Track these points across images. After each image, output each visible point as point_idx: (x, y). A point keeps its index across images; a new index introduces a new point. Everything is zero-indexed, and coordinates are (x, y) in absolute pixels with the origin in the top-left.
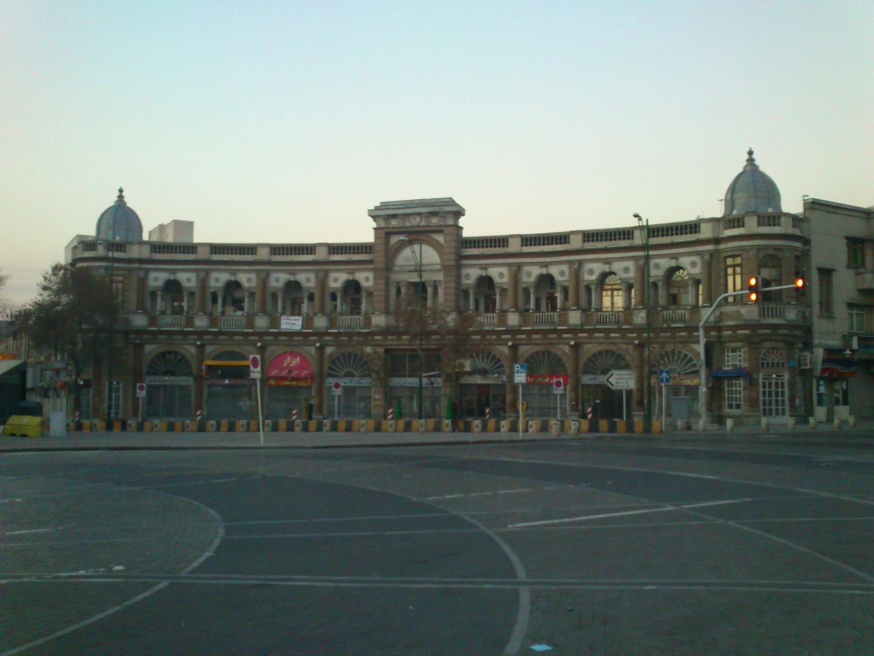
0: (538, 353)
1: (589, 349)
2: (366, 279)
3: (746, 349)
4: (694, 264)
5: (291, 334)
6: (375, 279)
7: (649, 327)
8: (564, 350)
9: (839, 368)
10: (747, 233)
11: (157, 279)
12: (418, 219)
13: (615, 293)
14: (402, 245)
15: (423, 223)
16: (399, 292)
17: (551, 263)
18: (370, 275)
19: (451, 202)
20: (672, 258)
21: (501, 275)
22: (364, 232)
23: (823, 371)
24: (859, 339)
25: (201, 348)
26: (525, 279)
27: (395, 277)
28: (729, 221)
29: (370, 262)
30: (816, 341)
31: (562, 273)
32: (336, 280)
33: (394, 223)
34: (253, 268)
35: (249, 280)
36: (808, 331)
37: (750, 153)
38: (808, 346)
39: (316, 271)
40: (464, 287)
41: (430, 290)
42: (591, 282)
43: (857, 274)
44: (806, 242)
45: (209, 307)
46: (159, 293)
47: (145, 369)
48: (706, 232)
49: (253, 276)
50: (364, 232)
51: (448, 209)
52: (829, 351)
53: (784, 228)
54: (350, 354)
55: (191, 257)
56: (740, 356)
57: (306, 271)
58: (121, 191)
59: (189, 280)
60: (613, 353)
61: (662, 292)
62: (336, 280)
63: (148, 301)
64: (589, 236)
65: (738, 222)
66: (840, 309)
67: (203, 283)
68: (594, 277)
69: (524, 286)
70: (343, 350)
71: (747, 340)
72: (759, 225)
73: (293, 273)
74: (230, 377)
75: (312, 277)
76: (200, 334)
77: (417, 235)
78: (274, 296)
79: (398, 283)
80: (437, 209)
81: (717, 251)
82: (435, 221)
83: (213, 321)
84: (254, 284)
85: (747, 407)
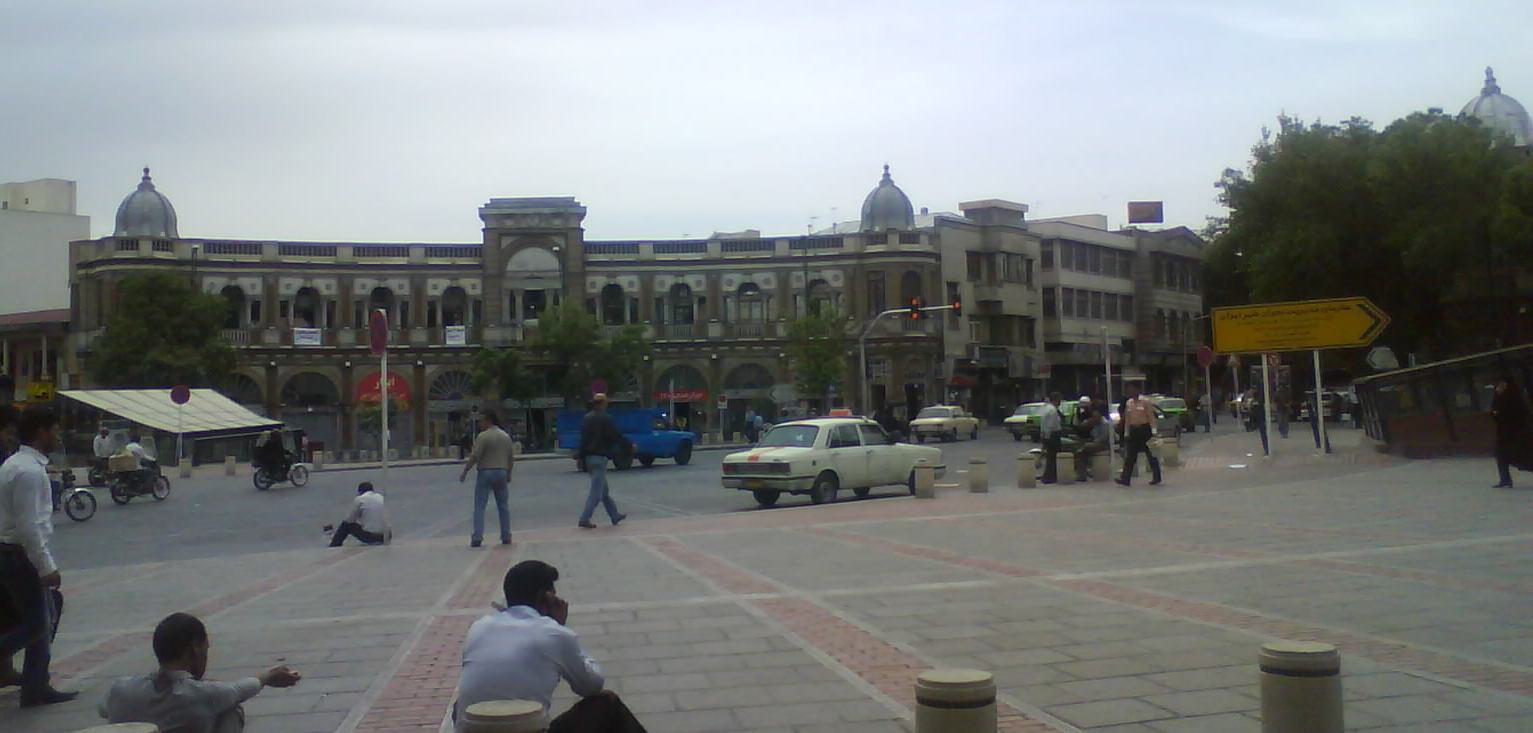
1: (731, 363)
2: (471, 286)
3: (890, 361)
4: (836, 278)
5: (309, 351)
6: (484, 288)
10: (890, 250)
13: (753, 304)
14: (515, 249)
15: (543, 225)
16: (513, 301)
18: (477, 282)
19: (569, 203)
20: (746, 274)
22: (472, 233)
23: (954, 379)
25: (271, 370)
26: (283, 291)
27: (508, 285)
28: (869, 237)
31: (699, 283)
35: (328, 287)
38: (941, 357)
43: (975, 286)
44: (938, 257)
47: (427, 392)
48: (849, 247)
49: (333, 282)
50: (472, 233)
51: (573, 210)
54: (455, 373)
55: (255, 259)
56: (884, 367)
57: (400, 275)
58: (147, 171)
59: (253, 286)
60: (756, 365)
61: (801, 301)
62: (435, 287)
65: (882, 238)
67: (270, 289)
68: (733, 288)
70: (449, 368)
72: (900, 242)
74: (312, 404)
75: (406, 283)
78: (284, 306)
79: (512, 292)
82: (557, 222)
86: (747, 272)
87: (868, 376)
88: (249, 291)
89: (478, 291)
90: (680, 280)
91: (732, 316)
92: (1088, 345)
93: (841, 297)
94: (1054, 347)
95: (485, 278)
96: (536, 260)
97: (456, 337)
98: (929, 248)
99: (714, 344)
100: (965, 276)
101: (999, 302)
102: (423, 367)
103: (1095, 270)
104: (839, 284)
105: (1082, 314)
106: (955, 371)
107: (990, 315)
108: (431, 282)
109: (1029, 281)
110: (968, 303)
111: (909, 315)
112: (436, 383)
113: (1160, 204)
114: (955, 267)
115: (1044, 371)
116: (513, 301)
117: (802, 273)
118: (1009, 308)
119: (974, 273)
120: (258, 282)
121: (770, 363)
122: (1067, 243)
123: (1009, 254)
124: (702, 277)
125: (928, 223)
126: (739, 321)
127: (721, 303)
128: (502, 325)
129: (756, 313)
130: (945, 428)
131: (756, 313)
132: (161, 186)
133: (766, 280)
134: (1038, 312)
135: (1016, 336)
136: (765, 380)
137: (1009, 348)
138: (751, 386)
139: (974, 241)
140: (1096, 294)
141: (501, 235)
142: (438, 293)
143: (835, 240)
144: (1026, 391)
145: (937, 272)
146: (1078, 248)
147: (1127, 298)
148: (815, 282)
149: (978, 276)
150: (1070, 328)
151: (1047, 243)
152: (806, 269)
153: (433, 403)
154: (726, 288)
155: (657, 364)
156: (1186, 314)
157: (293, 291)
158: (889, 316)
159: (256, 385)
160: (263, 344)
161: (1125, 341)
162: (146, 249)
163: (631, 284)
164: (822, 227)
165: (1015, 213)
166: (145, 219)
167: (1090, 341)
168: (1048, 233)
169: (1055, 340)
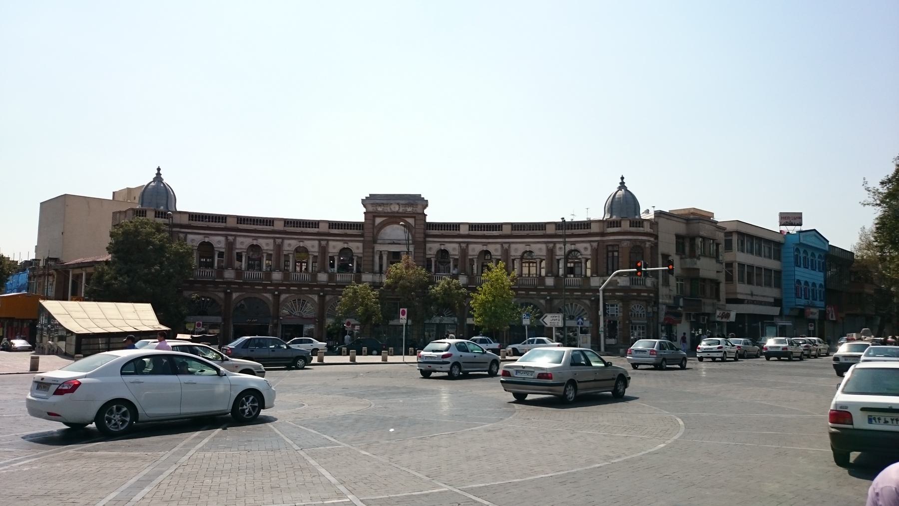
2: (356, 247)
6: (364, 248)
7: (555, 288)
9: (673, 318)
14: (383, 225)
15: (401, 210)
16: (381, 258)
17: (489, 243)
18: (360, 245)
22: (357, 215)
23: (665, 319)
24: (684, 300)
26: (470, 253)
27: (378, 248)
30: (660, 301)
33: (380, 209)
35: (267, 244)
37: (622, 178)
38: (656, 303)
40: (428, 256)
43: (681, 258)
44: (656, 237)
48: (595, 229)
50: (357, 215)
52: (668, 306)
53: (647, 228)
55: (222, 225)
63: (468, 265)
64: (515, 226)
69: (285, 253)
71: (621, 299)
73: (346, 242)
76: (229, 283)
77: (393, 218)
81: (603, 241)
86: (442, 243)
87: (605, 314)
89: (361, 251)
90: (485, 248)
96: (395, 232)
100: (675, 252)
101: (698, 269)
103: (759, 254)
105: (750, 282)
106: (666, 314)
107: (692, 278)
109: (717, 257)
110: (677, 268)
111: (636, 273)
113: (801, 214)
114: (667, 245)
116: (381, 258)
117: (562, 246)
118: (703, 274)
119: (680, 250)
122: (740, 234)
123: (704, 238)
124: (499, 246)
125: (651, 216)
128: (373, 272)
132: (167, 179)
134: (722, 278)
135: (708, 291)
137: (703, 300)
139: (681, 228)
141: (374, 217)
143: (587, 224)
145: (655, 246)
146: (747, 237)
147: (778, 273)
148: (571, 251)
149: (683, 252)
150: (742, 289)
151: (729, 234)
152: (565, 243)
164: (581, 217)
165: (704, 218)
168: (729, 228)
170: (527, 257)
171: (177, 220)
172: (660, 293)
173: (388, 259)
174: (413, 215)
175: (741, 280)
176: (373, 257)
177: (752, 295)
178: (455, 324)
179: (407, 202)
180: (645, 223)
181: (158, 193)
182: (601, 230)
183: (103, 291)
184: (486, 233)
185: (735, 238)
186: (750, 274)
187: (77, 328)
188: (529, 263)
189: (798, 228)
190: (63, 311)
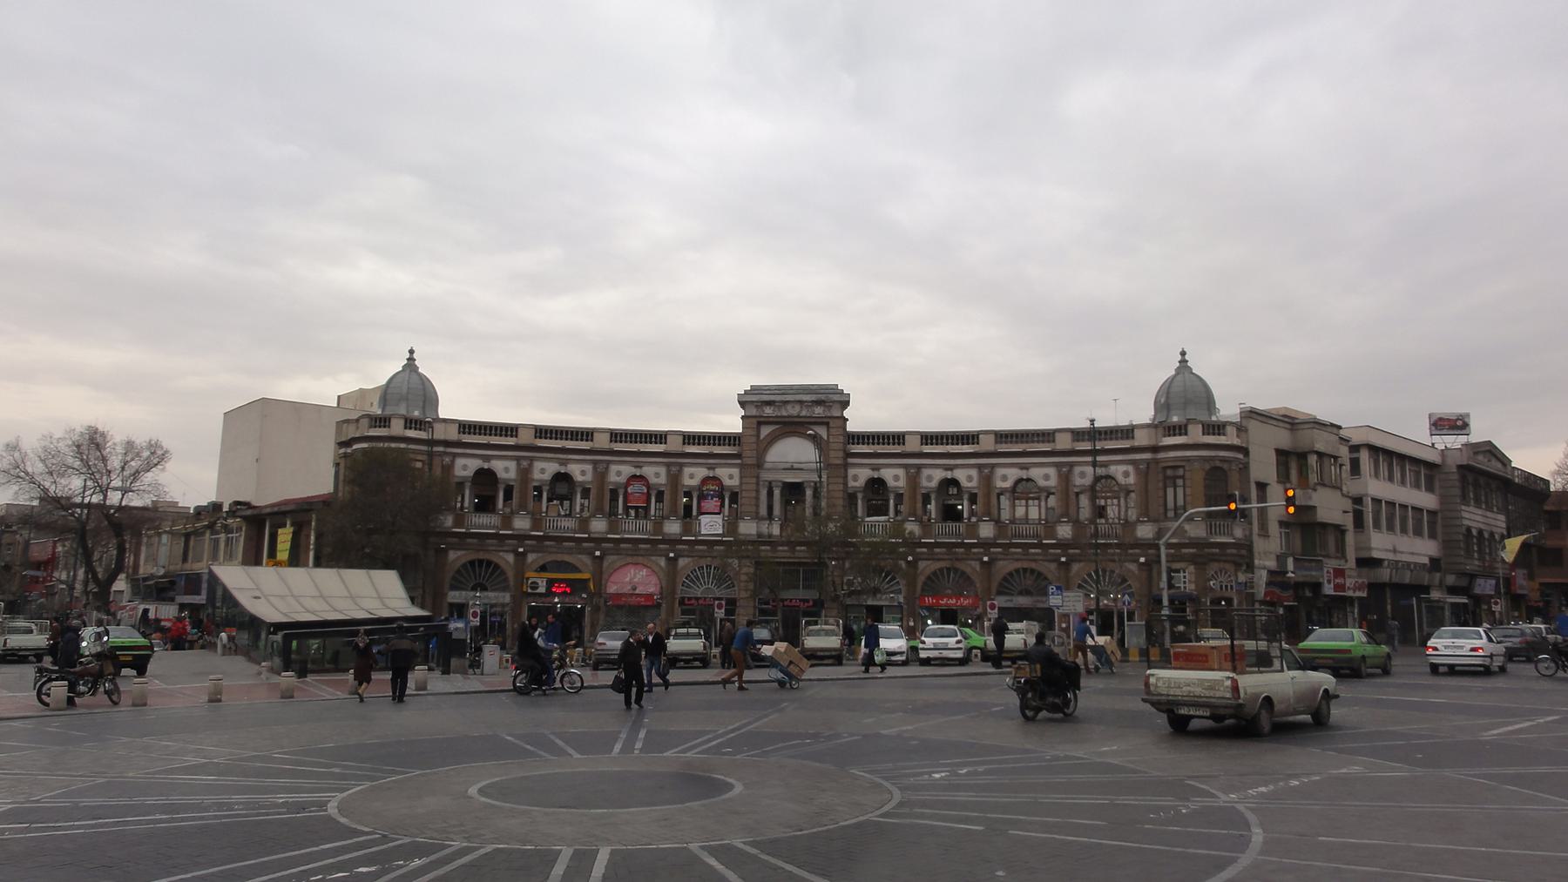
0: (941, 570)
1: (1005, 567)
8: (972, 567)
11: (466, 467)
12: (797, 408)
14: (773, 439)
15: (804, 413)
16: (770, 494)
17: (957, 466)
18: (735, 471)
19: (833, 390)
21: (896, 478)
22: (731, 422)
26: (924, 483)
27: (766, 476)
29: (738, 456)
30: (1256, 562)
32: (855, 478)
33: (768, 411)
34: (973, 461)
35: (583, 473)
36: (1249, 547)
38: (1250, 567)
39: (1057, 465)
41: (809, 493)
42: (693, 487)
45: (531, 504)
46: (468, 485)
48: (1141, 439)
49: (589, 468)
50: (731, 422)
51: (836, 398)
52: (1271, 572)
53: (1230, 438)
55: (511, 441)
59: (507, 470)
60: (1032, 571)
61: (1084, 501)
62: (692, 476)
65: (1181, 429)
66: (1274, 528)
68: (1008, 484)
71: (1192, 560)
75: (662, 471)
76: (521, 538)
77: (792, 428)
80: (823, 397)
81: (1157, 461)
83: (536, 524)
84: (589, 477)
85: (1364, 639)
86: (876, 468)
88: (501, 475)
90: (949, 475)
91: (1005, 515)
92: (1397, 562)
93: (1133, 495)
94: (1367, 563)
95: (741, 466)
96: (794, 454)
97: (711, 525)
98: (1236, 442)
99: (986, 545)
102: (524, 554)
104: (1052, 482)
106: (1269, 584)
107: (1304, 525)
108: (687, 471)
112: (458, 572)
114: (1263, 466)
115: (1360, 588)
116: (770, 494)
118: (1324, 515)
119: (1284, 477)
120: (512, 465)
121: (1050, 569)
122: (1374, 450)
123: (1320, 455)
126: (1013, 521)
127: (994, 501)
128: (757, 517)
129: (1034, 513)
130: (1354, 654)
131: (1034, 513)
133: (1044, 475)
134: (1348, 522)
136: (1039, 584)
138: (1027, 592)
139: (1283, 439)
140: (1404, 507)
141: (760, 424)
142: (695, 482)
143: (1127, 432)
144: (1331, 611)
145: (1245, 468)
147: (1432, 513)
150: (1381, 543)
152: (1094, 464)
153: (452, 593)
154: (1000, 484)
155: (922, 565)
156: (1492, 534)
157: (547, 476)
158: (1190, 519)
159: (503, 573)
160: (978, 537)
161: (1432, 560)
162: (397, 428)
163: (896, 478)
166: (1187, 403)
167: (1398, 557)
168: (1356, 439)
169: (1364, 555)
170: (1022, 491)
171: (440, 433)
172: (1256, 550)
173: (782, 495)
174: (824, 422)
175: (1377, 525)
176: (757, 491)
177: (1395, 551)
178: (900, 606)
179: (814, 398)
180: (1229, 428)
181: (412, 388)
182: (1153, 443)
183: (342, 549)
184: (880, 449)
185: (1364, 456)
186: (1395, 516)
187: (269, 612)
188: (1027, 499)
189: (1463, 439)
190: (248, 584)
